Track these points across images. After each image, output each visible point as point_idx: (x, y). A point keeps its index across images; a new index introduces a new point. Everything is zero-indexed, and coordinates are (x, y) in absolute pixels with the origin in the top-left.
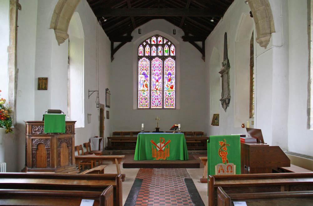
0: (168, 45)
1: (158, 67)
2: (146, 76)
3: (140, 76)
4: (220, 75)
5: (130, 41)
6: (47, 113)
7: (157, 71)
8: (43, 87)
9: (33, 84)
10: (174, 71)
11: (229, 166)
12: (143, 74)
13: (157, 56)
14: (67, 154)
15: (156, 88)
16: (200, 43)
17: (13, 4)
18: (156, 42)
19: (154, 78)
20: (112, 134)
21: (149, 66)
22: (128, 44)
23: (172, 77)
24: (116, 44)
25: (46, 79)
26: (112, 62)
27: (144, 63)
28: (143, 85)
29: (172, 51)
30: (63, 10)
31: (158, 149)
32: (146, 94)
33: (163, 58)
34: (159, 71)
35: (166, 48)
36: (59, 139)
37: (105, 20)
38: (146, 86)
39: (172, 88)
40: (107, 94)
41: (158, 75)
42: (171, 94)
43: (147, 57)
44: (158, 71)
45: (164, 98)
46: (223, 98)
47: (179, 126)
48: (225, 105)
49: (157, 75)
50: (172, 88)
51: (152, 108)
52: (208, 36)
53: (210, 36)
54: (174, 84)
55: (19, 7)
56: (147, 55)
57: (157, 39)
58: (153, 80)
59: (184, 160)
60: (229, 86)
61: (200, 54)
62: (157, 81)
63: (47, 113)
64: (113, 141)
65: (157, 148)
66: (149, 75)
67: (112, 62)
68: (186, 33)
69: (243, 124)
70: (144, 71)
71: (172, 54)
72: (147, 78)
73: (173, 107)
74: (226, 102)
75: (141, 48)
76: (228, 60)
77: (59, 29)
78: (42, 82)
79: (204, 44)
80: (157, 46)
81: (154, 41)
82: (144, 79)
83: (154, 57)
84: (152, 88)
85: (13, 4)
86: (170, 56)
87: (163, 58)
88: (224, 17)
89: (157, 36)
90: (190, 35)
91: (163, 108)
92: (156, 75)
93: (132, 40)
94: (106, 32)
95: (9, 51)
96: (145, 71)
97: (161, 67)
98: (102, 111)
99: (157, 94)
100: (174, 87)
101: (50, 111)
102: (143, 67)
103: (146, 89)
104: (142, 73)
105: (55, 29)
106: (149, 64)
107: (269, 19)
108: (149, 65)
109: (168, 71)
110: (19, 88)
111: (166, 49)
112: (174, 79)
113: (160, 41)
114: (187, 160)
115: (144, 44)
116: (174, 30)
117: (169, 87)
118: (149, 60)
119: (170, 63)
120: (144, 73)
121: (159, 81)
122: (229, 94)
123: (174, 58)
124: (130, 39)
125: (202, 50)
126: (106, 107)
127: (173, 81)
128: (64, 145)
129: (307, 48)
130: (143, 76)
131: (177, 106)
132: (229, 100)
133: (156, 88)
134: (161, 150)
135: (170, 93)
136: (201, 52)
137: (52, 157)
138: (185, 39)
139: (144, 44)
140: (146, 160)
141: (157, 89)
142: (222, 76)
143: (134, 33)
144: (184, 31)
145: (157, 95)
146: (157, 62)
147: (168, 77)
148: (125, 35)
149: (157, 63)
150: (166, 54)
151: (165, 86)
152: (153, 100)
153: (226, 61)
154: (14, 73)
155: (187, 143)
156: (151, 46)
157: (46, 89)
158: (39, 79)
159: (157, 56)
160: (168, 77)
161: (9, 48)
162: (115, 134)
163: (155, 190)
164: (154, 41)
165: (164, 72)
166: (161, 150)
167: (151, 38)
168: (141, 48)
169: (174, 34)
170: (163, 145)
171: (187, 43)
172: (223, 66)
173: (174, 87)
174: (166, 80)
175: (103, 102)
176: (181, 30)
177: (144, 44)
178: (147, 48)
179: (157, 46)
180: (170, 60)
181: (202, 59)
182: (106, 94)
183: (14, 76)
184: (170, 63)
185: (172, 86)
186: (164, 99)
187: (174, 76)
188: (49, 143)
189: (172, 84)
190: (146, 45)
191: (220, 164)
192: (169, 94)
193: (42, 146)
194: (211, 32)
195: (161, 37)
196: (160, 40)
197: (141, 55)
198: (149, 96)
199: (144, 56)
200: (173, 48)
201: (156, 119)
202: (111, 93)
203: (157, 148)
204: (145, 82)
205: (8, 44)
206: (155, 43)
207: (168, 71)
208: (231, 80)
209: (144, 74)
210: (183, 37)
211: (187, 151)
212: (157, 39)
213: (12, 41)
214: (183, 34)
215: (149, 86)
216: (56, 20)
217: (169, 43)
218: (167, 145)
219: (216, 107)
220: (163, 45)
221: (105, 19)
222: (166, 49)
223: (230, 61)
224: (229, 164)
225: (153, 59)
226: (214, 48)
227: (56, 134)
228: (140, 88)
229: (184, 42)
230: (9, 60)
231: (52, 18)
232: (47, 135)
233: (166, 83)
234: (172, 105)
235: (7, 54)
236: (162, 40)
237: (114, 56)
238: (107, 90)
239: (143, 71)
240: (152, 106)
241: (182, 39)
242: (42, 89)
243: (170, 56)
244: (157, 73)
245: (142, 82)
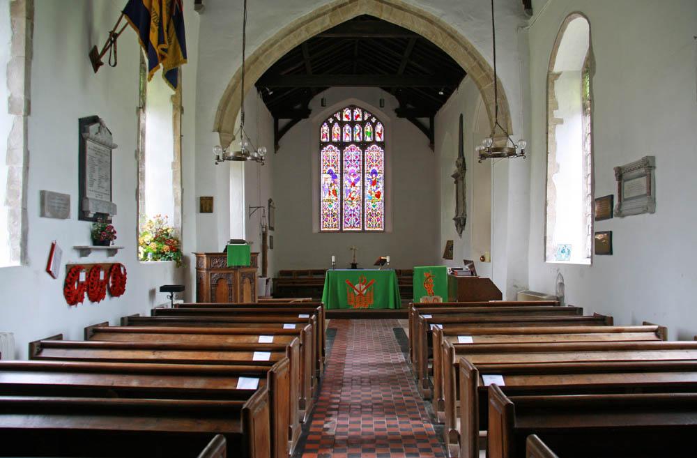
0: (371, 122)
1: (354, 161)
2: (334, 177)
3: (323, 176)
4: (454, 180)
5: (306, 117)
6: (229, 244)
7: (352, 168)
8: (208, 209)
9: (193, 206)
10: (382, 168)
11: (435, 298)
12: (328, 173)
13: (353, 142)
14: (249, 291)
15: (352, 196)
16: (425, 121)
17: (177, 109)
18: (350, 118)
19: (346, 178)
20: (119, 322)
21: (339, 159)
22: (303, 122)
23: (378, 177)
24: (283, 122)
25: (211, 199)
26: (275, 153)
27: (331, 154)
28: (330, 192)
29: (378, 133)
30: (229, 105)
31: (357, 293)
32: (335, 207)
33: (364, 145)
34: (357, 167)
35: (368, 128)
36: (242, 273)
37: (271, 93)
38: (335, 193)
39: (378, 196)
40: (271, 209)
41: (355, 175)
42: (377, 206)
43: (335, 144)
44: (355, 168)
45: (365, 213)
46: (457, 216)
47: (388, 259)
48: (460, 229)
49: (352, 174)
50: (378, 196)
51: (344, 230)
52: (438, 110)
53: (440, 110)
54: (381, 189)
55: (182, 110)
56: (335, 140)
57: (352, 112)
58: (346, 182)
59: (396, 308)
60: (464, 198)
61: (424, 139)
62: (354, 184)
63: (229, 244)
64: (279, 285)
65: (355, 291)
66: (339, 175)
67: (275, 153)
68: (402, 104)
69: (483, 257)
70: (331, 168)
71: (378, 139)
72: (335, 180)
73: (381, 229)
74: (461, 223)
75: (325, 128)
76: (464, 159)
77: (225, 132)
78: (206, 203)
79: (432, 122)
80: (352, 124)
81: (347, 116)
82: (330, 181)
83: (347, 144)
84: (344, 197)
85: (177, 109)
86: (374, 142)
87: (364, 145)
88: (459, 88)
89: (352, 108)
90: (410, 106)
91: (363, 230)
92: (350, 174)
93: (310, 116)
94: (267, 106)
95: (173, 167)
96: (332, 168)
97: (359, 160)
98: (264, 235)
99: (352, 207)
100: (382, 195)
101: (233, 241)
102: (329, 161)
103: (335, 198)
104: (327, 171)
105: (219, 131)
106: (339, 155)
107: (506, 116)
108: (339, 157)
109: (372, 168)
110: (184, 213)
111: (369, 130)
112: (382, 181)
113: (358, 116)
114: (399, 309)
115: (331, 120)
116: (380, 100)
117: (374, 195)
118: (338, 149)
119: (375, 153)
120: (330, 170)
121: (356, 185)
122: (464, 211)
123: (381, 144)
124: (306, 113)
125: (430, 133)
126: (270, 229)
127: (381, 185)
128: (247, 280)
129: (545, 162)
130: (329, 176)
131: (386, 228)
132: (465, 220)
133: (352, 196)
134: (361, 295)
135: (376, 206)
136: (428, 136)
137: (235, 294)
138: (400, 113)
139: (331, 120)
140: (338, 308)
141: (353, 198)
142: (456, 182)
143: (314, 104)
144: (399, 101)
145: (352, 209)
146: (353, 153)
147: (371, 177)
148: (298, 107)
149: (352, 153)
150: (368, 139)
151: (367, 192)
152: (345, 217)
153: (461, 160)
154: (180, 195)
155: (400, 287)
156: (342, 124)
157: (211, 211)
158: (202, 199)
159: (353, 142)
160: (371, 177)
161: (173, 164)
162: (282, 273)
163: (352, 393)
164: (347, 116)
165: (366, 169)
166: (361, 295)
167: (342, 111)
168: (325, 128)
169: (381, 107)
170: (363, 287)
171: (405, 120)
172: (458, 166)
173: (382, 195)
174: (367, 183)
175: (266, 222)
176: (394, 97)
177: (331, 122)
178: (336, 127)
179: (352, 124)
180: (375, 149)
181: (430, 148)
182: (269, 209)
183: (180, 199)
184: (374, 153)
185: (379, 193)
186: (366, 216)
187: (382, 175)
188: (231, 277)
189: (379, 190)
190: (333, 123)
191: (426, 297)
192: (374, 206)
193: (223, 281)
194: (444, 106)
195: (360, 108)
196: (358, 113)
197: (324, 140)
198: (339, 210)
199: (331, 142)
200: (379, 127)
201: (352, 249)
202: (275, 206)
203: (355, 291)
204: (333, 187)
205: (172, 159)
206: (349, 119)
207: (372, 168)
208: (467, 188)
209: (330, 172)
210: (396, 111)
211: (401, 300)
212: (352, 112)
213: (176, 154)
214: (397, 104)
215: (338, 193)
216: (220, 120)
217: (374, 120)
218: (369, 287)
219: (448, 231)
220: (363, 124)
221: (271, 90)
222: (369, 130)
223: (466, 161)
224: (435, 297)
225: (347, 148)
226: (447, 134)
227: (239, 267)
228: (325, 196)
229: (398, 118)
230: (174, 178)
231: (216, 118)
232: (229, 268)
233: (369, 188)
234: (379, 224)
235: (171, 171)
236: (361, 115)
237: (280, 143)
238: (270, 201)
239: (329, 168)
240: (345, 228)
241: (396, 114)
242: (206, 212)
243: (374, 142)
244: (353, 171)
245: (327, 187)
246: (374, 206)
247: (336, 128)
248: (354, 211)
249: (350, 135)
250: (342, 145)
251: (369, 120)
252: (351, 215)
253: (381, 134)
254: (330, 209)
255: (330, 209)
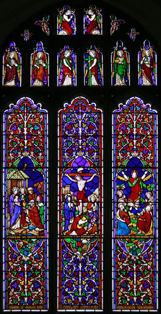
0: (37, 111)
2: (35, 177)
10: (154, 156)
12: (20, 168)
13: (81, 88)
33: (107, 97)
35: (120, 56)
39: (144, 225)
43: (36, 93)
50: (144, 225)
66: (46, 174)
81: (66, 25)
86: (134, 88)
92: (75, 171)
97: (95, 136)
104: (16, 163)
113: (94, 25)
141: (81, 233)
146: (81, 118)
156: (54, 46)
173: (155, 223)
192: (134, 252)
209: (25, 165)
220: (105, 45)
234: (147, 297)
240: (62, 306)
244: (82, 162)
246: (134, 252)
247: (40, 55)
248: (84, 262)
249: (75, 72)
250: (53, 97)
251: (121, 35)
252: (76, 274)
253: (151, 70)
254: (26, 259)
255: (26, 259)
